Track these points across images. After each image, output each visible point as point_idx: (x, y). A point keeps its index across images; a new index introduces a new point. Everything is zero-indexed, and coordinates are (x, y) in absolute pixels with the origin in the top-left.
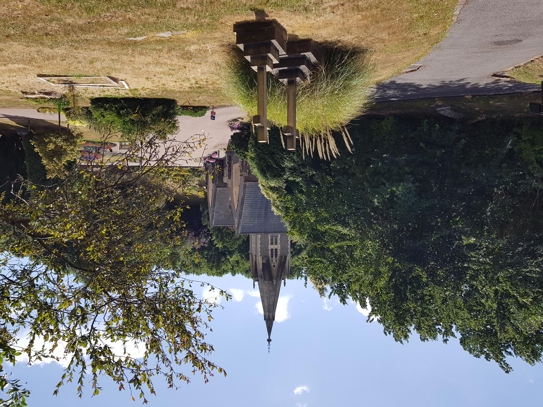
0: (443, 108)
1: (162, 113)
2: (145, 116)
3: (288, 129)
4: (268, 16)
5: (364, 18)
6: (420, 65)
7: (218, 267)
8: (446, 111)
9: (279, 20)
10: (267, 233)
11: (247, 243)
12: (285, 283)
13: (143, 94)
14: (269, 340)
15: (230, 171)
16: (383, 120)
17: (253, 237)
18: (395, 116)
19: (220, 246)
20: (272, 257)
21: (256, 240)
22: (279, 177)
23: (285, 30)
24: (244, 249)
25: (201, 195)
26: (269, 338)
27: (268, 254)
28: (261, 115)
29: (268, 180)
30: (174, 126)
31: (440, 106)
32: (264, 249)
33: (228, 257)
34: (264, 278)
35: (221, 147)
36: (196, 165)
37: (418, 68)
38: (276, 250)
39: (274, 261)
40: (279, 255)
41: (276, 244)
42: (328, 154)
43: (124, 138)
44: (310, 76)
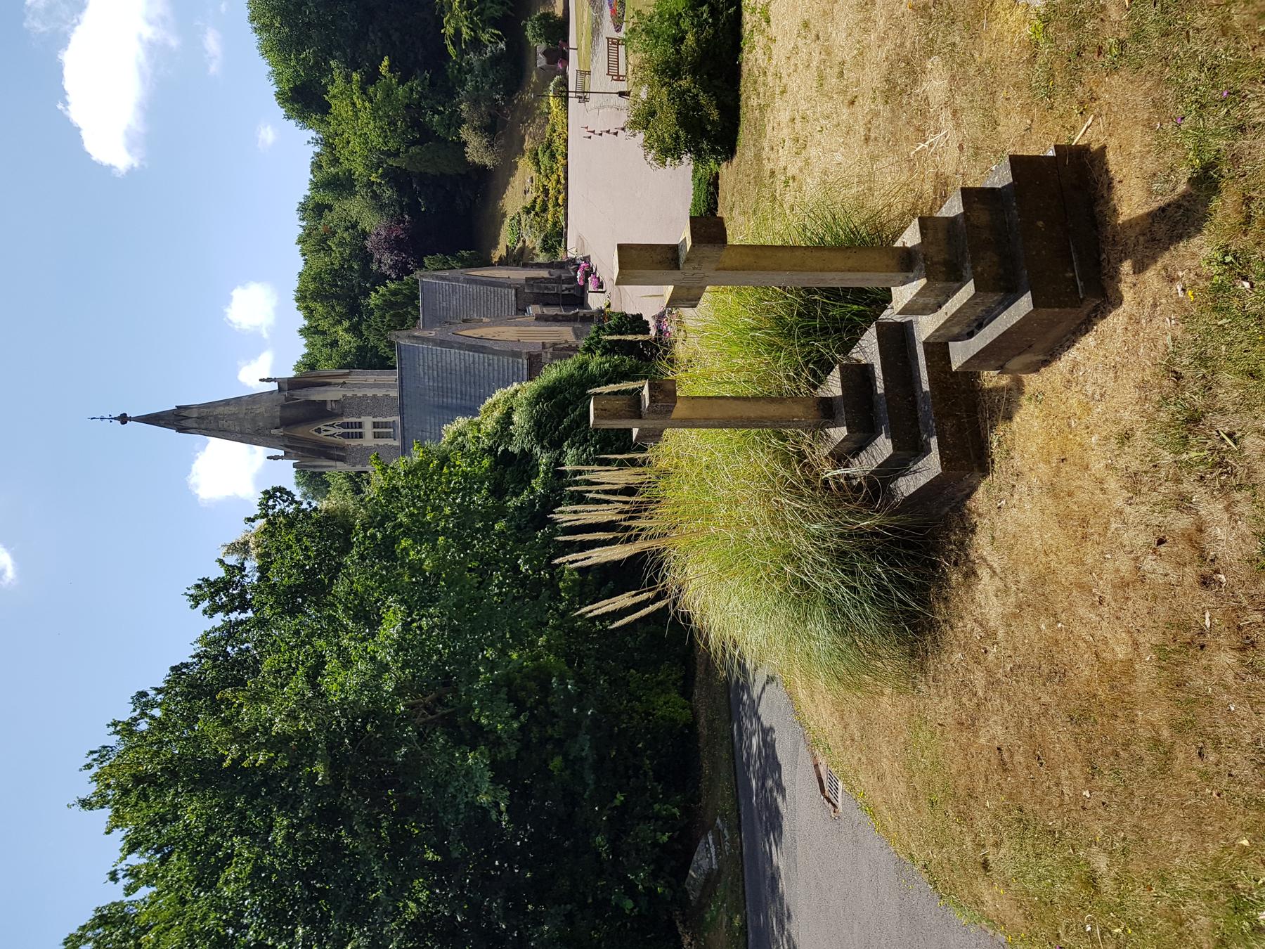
0: (713, 850)
1: (700, 120)
2: (694, 72)
3: (665, 393)
4: (1139, 268)
5: (1118, 676)
6: (839, 805)
7: (319, 296)
8: (706, 858)
9: (1115, 321)
10: (402, 415)
11: (383, 363)
12: (276, 458)
13: (753, 58)
14: (124, 419)
15: (556, 319)
16: (682, 695)
17: (391, 377)
18: (692, 726)
19: (374, 300)
20: (342, 425)
21: (384, 386)
22: (537, 436)
23: (1046, 363)
24: (369, 359)
25: (500, 252)
26: (130, 419)
27: (348, 416)
28: (726, 258)
29: (530, 404)
30: (667, 151)
31: (718, 842)
32: (361, 405)
33: (346, 324)
34: (288, 406)
35: (614, 296)
36: (571, 243)
37: (829, 800)
38: (361, 436)
39: (332, 431)
40: (347, 442)
41: (376, 436)
42: (579, 537)
43: (635, 20)
44: (848, 478)
